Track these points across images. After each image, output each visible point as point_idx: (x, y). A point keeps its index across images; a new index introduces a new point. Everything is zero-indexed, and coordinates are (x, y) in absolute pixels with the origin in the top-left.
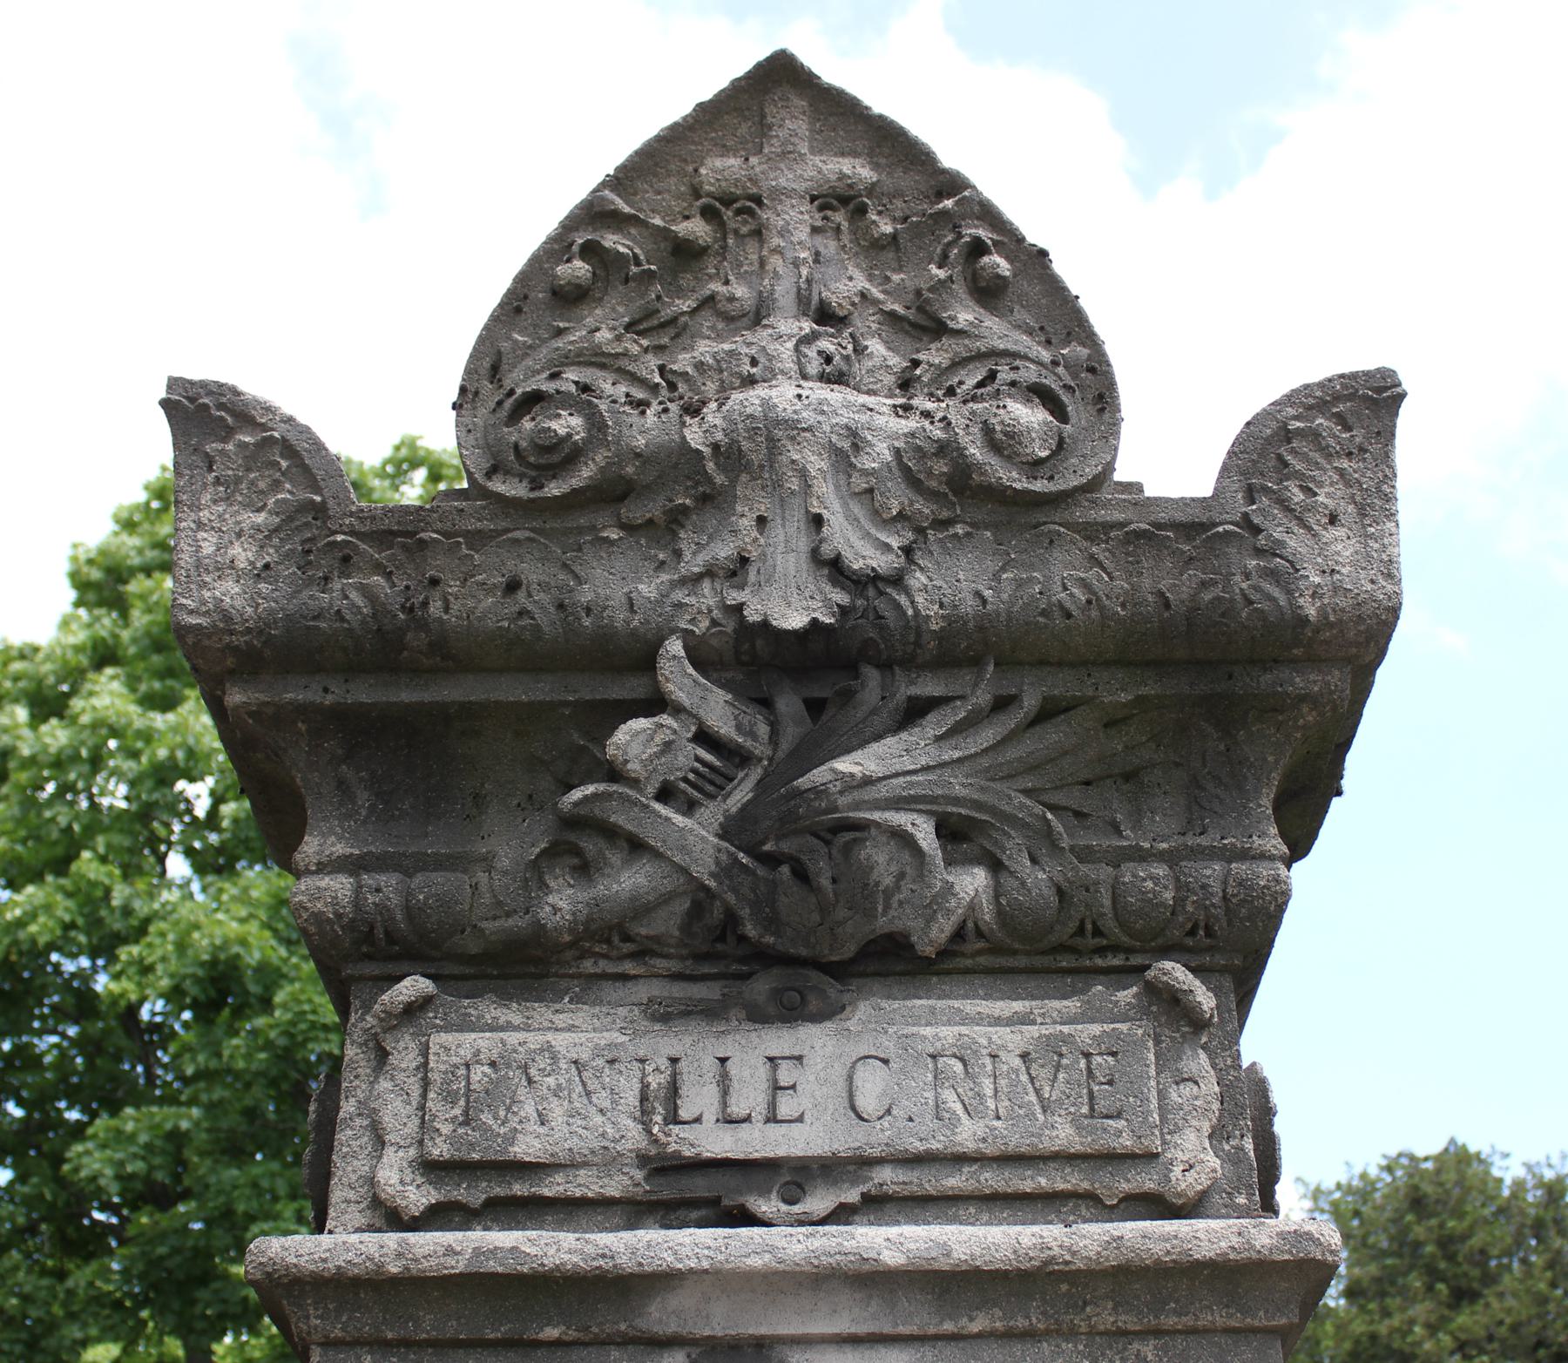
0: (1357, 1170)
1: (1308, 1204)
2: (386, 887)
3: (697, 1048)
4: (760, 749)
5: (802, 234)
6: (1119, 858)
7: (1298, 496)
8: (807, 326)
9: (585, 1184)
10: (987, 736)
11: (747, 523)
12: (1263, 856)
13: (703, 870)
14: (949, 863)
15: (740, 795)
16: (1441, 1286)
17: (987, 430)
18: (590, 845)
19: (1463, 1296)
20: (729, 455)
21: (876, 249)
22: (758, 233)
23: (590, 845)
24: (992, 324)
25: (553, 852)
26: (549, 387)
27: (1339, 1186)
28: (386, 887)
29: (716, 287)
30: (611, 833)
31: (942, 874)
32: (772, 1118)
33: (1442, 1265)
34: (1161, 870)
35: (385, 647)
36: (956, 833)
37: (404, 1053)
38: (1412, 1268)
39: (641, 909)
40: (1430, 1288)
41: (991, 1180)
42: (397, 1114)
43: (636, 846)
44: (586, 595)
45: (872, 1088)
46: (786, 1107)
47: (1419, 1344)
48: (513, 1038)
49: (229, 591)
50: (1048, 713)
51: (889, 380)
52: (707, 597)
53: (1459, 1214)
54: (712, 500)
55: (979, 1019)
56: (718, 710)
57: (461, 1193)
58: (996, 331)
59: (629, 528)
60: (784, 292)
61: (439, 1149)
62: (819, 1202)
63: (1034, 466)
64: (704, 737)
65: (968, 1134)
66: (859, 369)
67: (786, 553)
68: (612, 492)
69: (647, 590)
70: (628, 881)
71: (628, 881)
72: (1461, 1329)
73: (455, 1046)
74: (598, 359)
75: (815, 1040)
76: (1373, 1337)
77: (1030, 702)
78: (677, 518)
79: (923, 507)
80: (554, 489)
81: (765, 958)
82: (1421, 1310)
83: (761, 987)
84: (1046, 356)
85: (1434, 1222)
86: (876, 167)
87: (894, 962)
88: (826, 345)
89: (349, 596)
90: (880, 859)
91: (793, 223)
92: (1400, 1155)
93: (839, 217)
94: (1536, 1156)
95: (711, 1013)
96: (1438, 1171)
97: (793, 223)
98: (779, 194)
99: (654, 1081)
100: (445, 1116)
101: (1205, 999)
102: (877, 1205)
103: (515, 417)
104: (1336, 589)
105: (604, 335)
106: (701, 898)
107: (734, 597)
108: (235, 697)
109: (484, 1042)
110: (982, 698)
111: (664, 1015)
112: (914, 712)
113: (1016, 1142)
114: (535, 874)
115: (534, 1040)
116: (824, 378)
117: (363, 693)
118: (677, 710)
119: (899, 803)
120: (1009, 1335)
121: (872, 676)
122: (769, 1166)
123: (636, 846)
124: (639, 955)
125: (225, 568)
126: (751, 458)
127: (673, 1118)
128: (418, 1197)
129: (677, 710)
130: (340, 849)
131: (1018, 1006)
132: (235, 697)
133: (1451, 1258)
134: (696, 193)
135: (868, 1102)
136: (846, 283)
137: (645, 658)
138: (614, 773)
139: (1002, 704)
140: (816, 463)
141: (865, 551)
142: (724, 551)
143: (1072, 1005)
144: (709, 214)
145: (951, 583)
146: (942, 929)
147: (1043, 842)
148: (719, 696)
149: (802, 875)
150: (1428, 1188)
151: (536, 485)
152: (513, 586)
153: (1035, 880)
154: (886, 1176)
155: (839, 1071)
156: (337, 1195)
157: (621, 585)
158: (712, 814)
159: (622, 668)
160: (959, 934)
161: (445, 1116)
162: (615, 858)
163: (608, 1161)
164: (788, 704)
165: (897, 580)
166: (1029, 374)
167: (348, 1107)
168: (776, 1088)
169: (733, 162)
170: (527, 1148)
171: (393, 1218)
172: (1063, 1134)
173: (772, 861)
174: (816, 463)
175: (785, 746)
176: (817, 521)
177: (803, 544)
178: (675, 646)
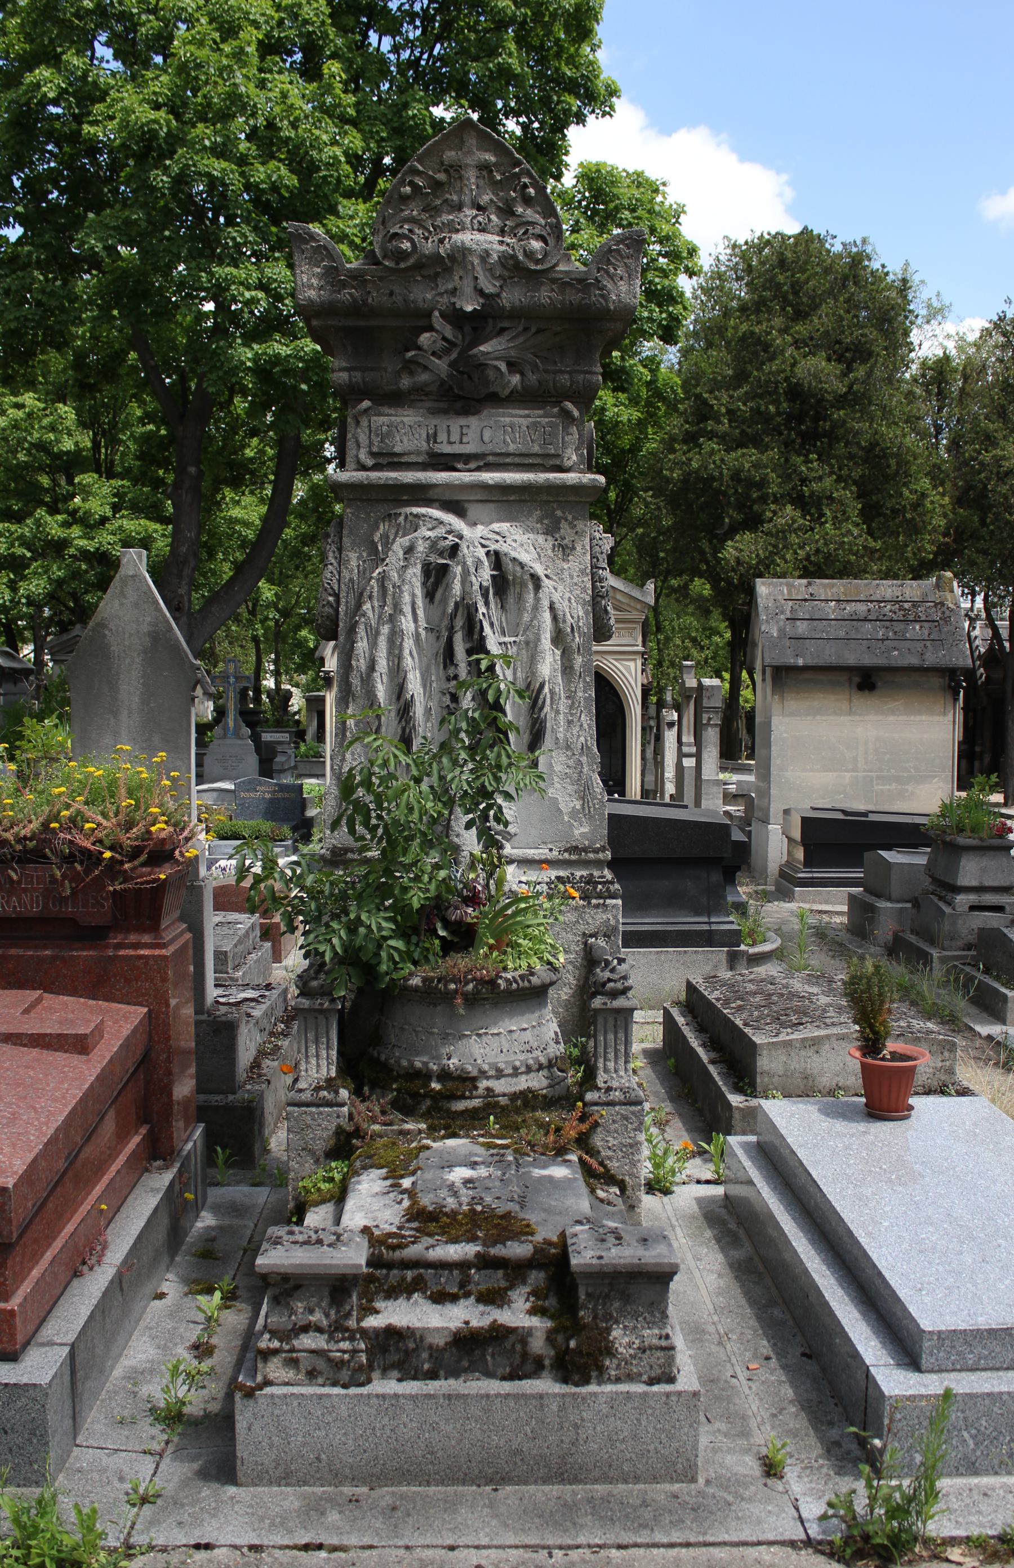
0: (758, 234)
1: (729, 251)
2: (357, 376)
3: (442, 423)
4: (459, 342)
5: (473, 180)
6: (555, 372)
7: (612, 270)
8: (475, 212)
9: (413, 459)
10: (521, 339)
11: (457, 278)
12: (596, 373)
13: (443, 376)
14: (510, 372)
15: (454, 355)
16: (789, 309)
17: (525, 251)
18: (413, 367)
19: (800, 315)
20: (452, 257)
21: (495, 185)
22: (461, 178)
23: (413, 367)
24: (529, 211)
25: (403, 368)
26: (399, 231)
27: (746, 243)
28: (357, 376)
29: (448, 196)
30: (418, 364)
31: (508, 377)
32: (461, 442)
33: (791, 297)
34: (567, 377)
35: (356, 309)
36: (511, 365)
37: (364, 423)
38: (775, 297)
39: (427, 384)
40: (783, 309)
41: (517, 460)
42: (363, 439)
43: (426, 368)
44: (412, 297)
45: (487, 435)
46: (465, 440)
47: (774, 340)
48: (393, 418)
49: (312, 294)
50: (538, 332)
51: (497, 229)
52: (445, 299)
53: (803, 271)
54: (448, 271)
55: (516, 416)
56: (448, 331)
57: (381, 461)
58: (530, 214)
59: (423, 276)
60: (467, 199)
61: (375, 449)
62: (473, 465)
63: (537, 262)
64: (444, 339)
65: (512, 448)
66: (489, 227)
67: (467, 287)
68: (419, 266)
69: (429, 296)
70: (424, 377)
71: (424, 377)
72: (797, 332)
73: (379, 421)
74: (412, 220)
75: (473, 422)
76: (752, 333)
77: (533, 330)
78: (437, 275)
79: (506, 273)
80: (402, 265)
81: (461, 397)
82: (778, 321)
83: (458, 405)
84: (543, 222)
85: (789, 273)
86: (496, 155)
87: (496, 400)
88: (480, 218)
89: (346, 295)
90: (491, 374)
91: (471, 176)
92: (777, 233)
93: (485, 173)
94: (849, 239)
95: (445, 412)
96: (796, 244)
97: (471, 176)
98: (466, 165)
99: (431, 432)
100: (376, 441)
101: (576, 413)
102: (488, 467)
103: (390, 241)
104: (620, 301)
105: (415, 213)
106: (443, 382)
107: (453, 300)
108: (315, 323)
109: (385, 419)
110: (520, 329)
111: (433, 412)
112: (502, 331)
113: (524, 451)
114: (398, 374)
115: (398, 419)
116: (479, 230)
117: (350, 323)
118: (437, 331)
119: (497, 359)
120: (520, 501)
121: (490, 321)
122: (460, 455)
123: (426, 368)
124: (426, 395)
125: (311, 286)
126: (460, 254)
127: (435, 442)
128: (370, 462)
129: (437, 331)
130: (344, 364)
131: (527, 412)
132: (315, 323)
133: (796, 293)
134: (442, 163)
135: (486, 439)
136: (485, 199)
137: (429, 315)
138: (419, 348)
139: (526, 329)
140: (476, 261)
141: (490, 289)
142: (450, 286)
143: (541, 412)
144: (446, 171)
145: (512, 297)
146: (507, 392)
147: (535, 368)
148: (449, 327)
149: (470, 377)
150: (789, 254)
151: (397, 263)
152: (391, 294)
153: (533, 378)
154: (491, 459)
155: (479, 431)
156: (348, 460)
157: (422, 295)
158: (447, 360)
159: (422, 320)
160: (512, 392)
161: (376, 441)
162: (420, 370)
163: (418, 453)
164: (467, 329)
165: (498, 295)
166: (538, 230)
167: (349, 436)
168: (462, 434)
169: (453, 153)
170: (397, 449)
171: (363, 468)
172: (536, 449)
173: (462, 373)
174: (476, 261)
175: (467, 342)
176: (476, 278)
177: (472, 284)
178: (436, 313)
